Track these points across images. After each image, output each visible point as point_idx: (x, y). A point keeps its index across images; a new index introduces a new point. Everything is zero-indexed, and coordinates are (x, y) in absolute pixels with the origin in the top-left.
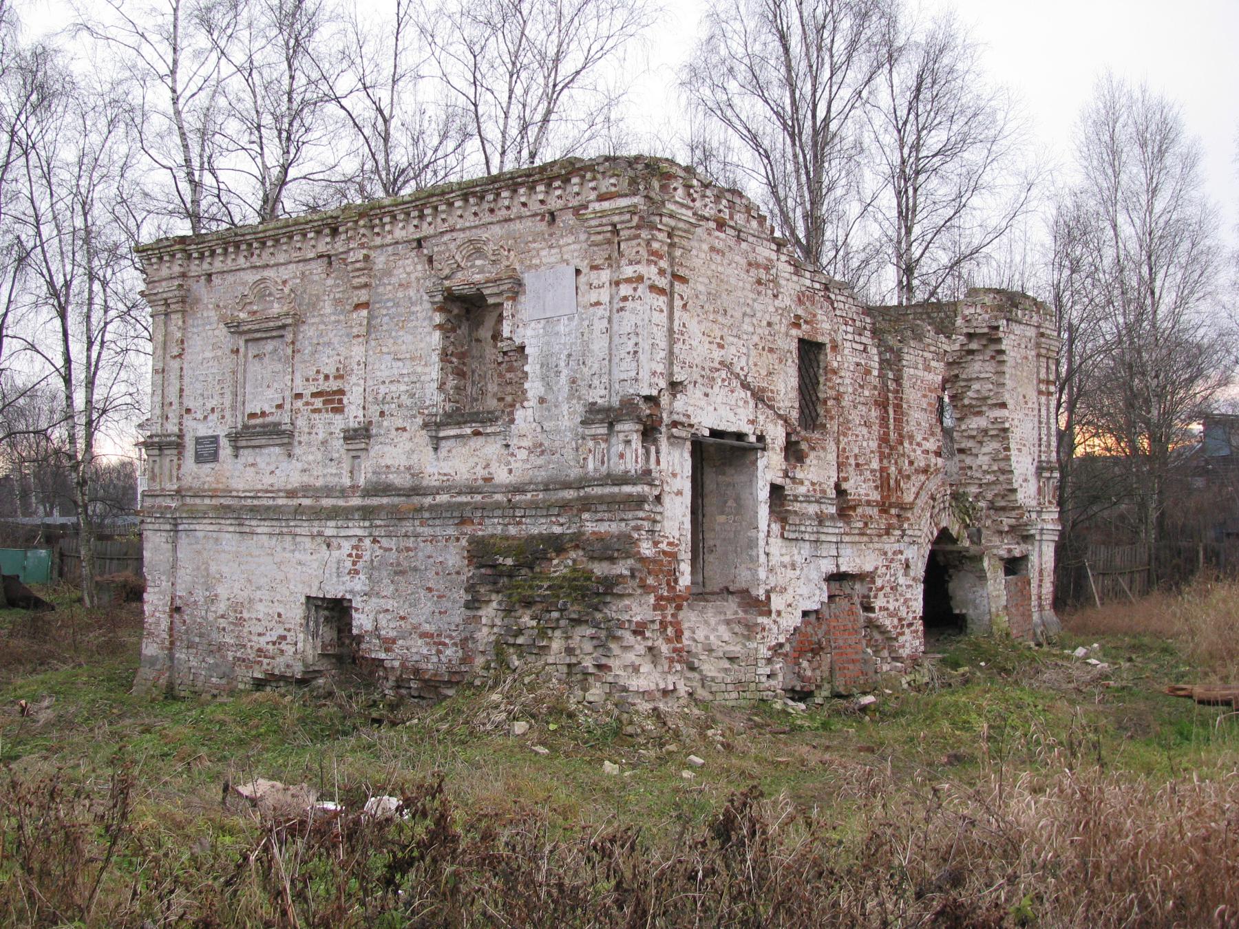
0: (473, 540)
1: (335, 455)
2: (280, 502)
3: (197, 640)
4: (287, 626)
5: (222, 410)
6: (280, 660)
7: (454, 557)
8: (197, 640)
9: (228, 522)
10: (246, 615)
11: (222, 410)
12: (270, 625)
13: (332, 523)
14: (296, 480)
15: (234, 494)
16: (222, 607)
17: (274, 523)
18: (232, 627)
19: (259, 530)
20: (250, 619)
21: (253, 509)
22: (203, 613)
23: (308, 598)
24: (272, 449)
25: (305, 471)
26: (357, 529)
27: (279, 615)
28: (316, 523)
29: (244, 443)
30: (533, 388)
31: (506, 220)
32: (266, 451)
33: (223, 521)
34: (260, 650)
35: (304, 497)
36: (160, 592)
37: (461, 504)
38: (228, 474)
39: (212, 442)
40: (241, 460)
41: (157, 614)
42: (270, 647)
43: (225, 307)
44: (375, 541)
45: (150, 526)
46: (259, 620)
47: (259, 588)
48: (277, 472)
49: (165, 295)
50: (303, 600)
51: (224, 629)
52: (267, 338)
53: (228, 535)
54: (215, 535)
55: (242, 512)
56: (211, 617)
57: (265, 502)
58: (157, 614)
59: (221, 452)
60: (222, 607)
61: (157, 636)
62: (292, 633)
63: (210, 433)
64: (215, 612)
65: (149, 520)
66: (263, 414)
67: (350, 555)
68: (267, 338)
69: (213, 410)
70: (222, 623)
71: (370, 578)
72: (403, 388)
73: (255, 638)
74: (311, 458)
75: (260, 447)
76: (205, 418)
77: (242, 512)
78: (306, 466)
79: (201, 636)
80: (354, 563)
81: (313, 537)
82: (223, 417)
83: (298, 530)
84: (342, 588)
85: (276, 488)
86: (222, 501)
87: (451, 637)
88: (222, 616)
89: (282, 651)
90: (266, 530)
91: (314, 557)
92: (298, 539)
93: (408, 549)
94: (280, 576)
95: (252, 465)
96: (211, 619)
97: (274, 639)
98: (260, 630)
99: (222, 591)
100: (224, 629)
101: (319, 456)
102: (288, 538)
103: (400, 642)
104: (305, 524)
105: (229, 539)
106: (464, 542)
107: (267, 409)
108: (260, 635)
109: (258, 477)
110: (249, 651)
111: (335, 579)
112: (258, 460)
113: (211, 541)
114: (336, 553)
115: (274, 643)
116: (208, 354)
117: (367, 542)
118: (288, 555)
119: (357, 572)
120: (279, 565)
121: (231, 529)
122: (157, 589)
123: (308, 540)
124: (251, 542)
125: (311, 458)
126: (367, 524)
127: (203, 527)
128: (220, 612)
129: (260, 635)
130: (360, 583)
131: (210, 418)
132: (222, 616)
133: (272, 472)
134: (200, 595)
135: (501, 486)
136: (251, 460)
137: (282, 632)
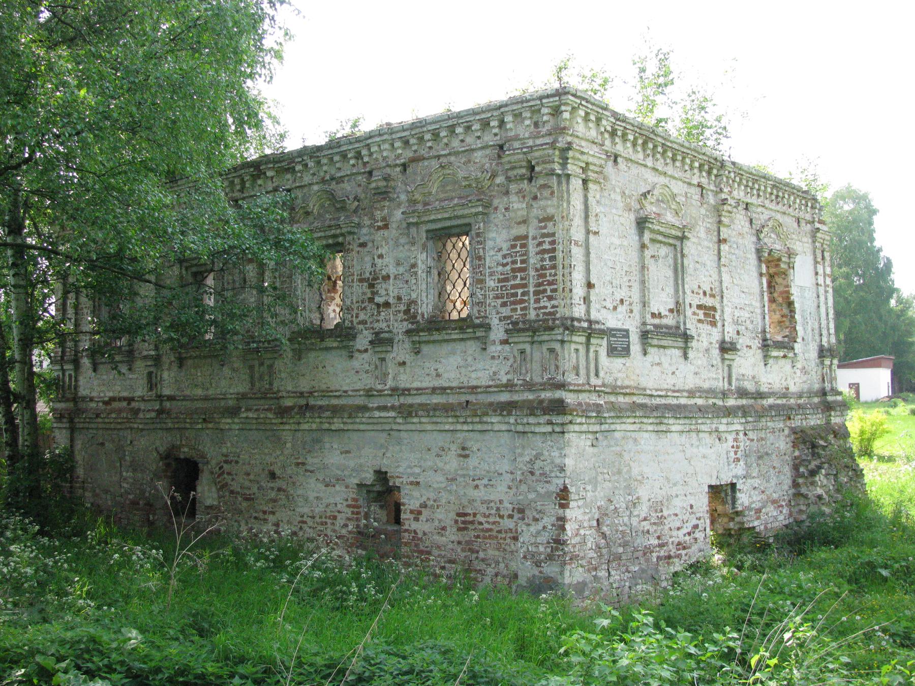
0: (794, 431)
1: (715, 363)
2: (683, 401)
3: (621, 550)
4: (698, 515)
5: (631, 304)
6: (695, 548)
7: (782, 443)
8: (621, 550)
9: (651, 421)
10: (665, 513)
11: (631, 304)
12: (685, 518)
13: (724, 421)
14: (691, 382)
15: (648, 392)
16: (643, 510)
17: (687, 421)
18: (655, 527)
19: (673, 428)
20: (669, 515)
21: (668, 407)
22: (626, 519)
23: (710, 487)
24: (673, 350)
25: (696, 373)
26: (737, 425)
27: (692, 507)
28: (715, 421)
29: (655, 342)
30: (800, 333)
31: (784, 213)
32: (668, 351)
33: (645, 420)
34: (679, 544)
35: (700, 397)
36: (586, 505)
37: (778, 405)
38: (637, 372)
39: (624, 336)
40: (649, 358)
41: (582, 532)
42: (687, 538)
43: (630, 197)
44: (745, 434)
45: (577, 428)
46: (676, 515)
47: (675, 485)
48: (677, 373)
49: (591, 160)
50: (706, 489)
51: (648, 532)
52: (661, 242)
53: (646, 435)
54: (633, 434)
55: (659, 411)
56: (635, 522)
57: (670, 401)
58: (582, 532)
59: (631, 347)
60: (643, 510)
61: (583, 558)
62: (702, 521)
63: (619, 325)
64: (638, 516)
65: (579, 420)
66: (660, 316)
67: (733, 447)
68: (661, 242)
69: (622, 301)
70: (646, 525)
71: (746, 464)
72: (747, 315)
73: (675, 533)
74: (700, 362)
75: (664, 347)
76: (615, 308)
77: (659, 411)
78: (697, 370)
79: (625, 545)
80: (736, 453)
81: (710, 433)
82: (631, 311)
83: (703, 427)
84: (731, 474)
85: (677, 388)
86: (635, 399)
87: (784, 500)
88: (645, 519)
89: (696, 539)
90: (679, 428)
91: (712, 450)
92: (701, 435)
93: (762, 439)
94: (691, 471)
95: (658, 364)
96: (635, 523)
97: (689, 530)
98: (678, 524)
99: (643, 492)
100: (648, 532)
101: (705, 363)
102: (694, 435)
103: (763, 510)
104: (708, 421)
105: (647, 440)
106: (787, 432)
107: (664, 312)
108: (678, 529)
109: (664, 376)
110: (671, 546)
111: (726, 468)
112: (663, 359)
113: (631, 441)
114: (725, 445)
115: (689, 534)
116: (617, 242)
117: (741, 434)
118: (695, 450)
119: (738, 460)
120: (689, 460)
121: (650, 428)
122: (581, 503)
123: (707, 435)
124: (665, 440)
125: (700, 362)
126: (743, 420)
127: (628, 425)
128: (643, 515)
129: (678, 529)
130: (740, 469)
131: (620, 309)
132: (645, 519)
133: (673, 373)
134: (621, 502)
135: (793, 394)
136: (657, 361)
137: (695, 522)
